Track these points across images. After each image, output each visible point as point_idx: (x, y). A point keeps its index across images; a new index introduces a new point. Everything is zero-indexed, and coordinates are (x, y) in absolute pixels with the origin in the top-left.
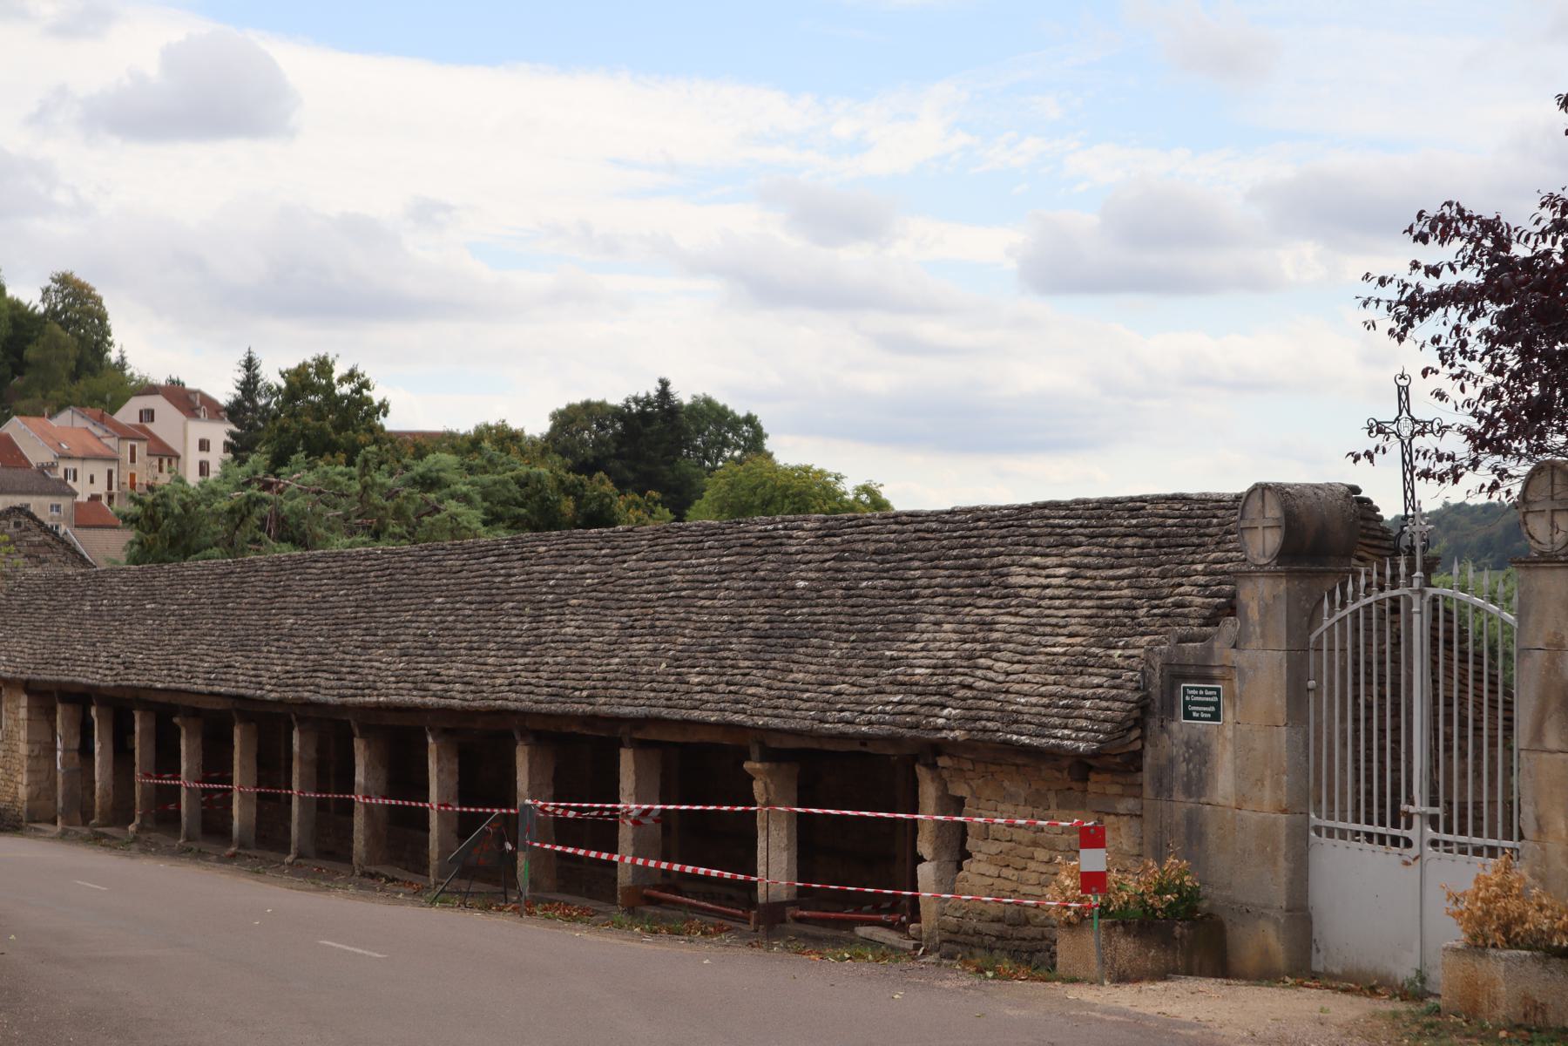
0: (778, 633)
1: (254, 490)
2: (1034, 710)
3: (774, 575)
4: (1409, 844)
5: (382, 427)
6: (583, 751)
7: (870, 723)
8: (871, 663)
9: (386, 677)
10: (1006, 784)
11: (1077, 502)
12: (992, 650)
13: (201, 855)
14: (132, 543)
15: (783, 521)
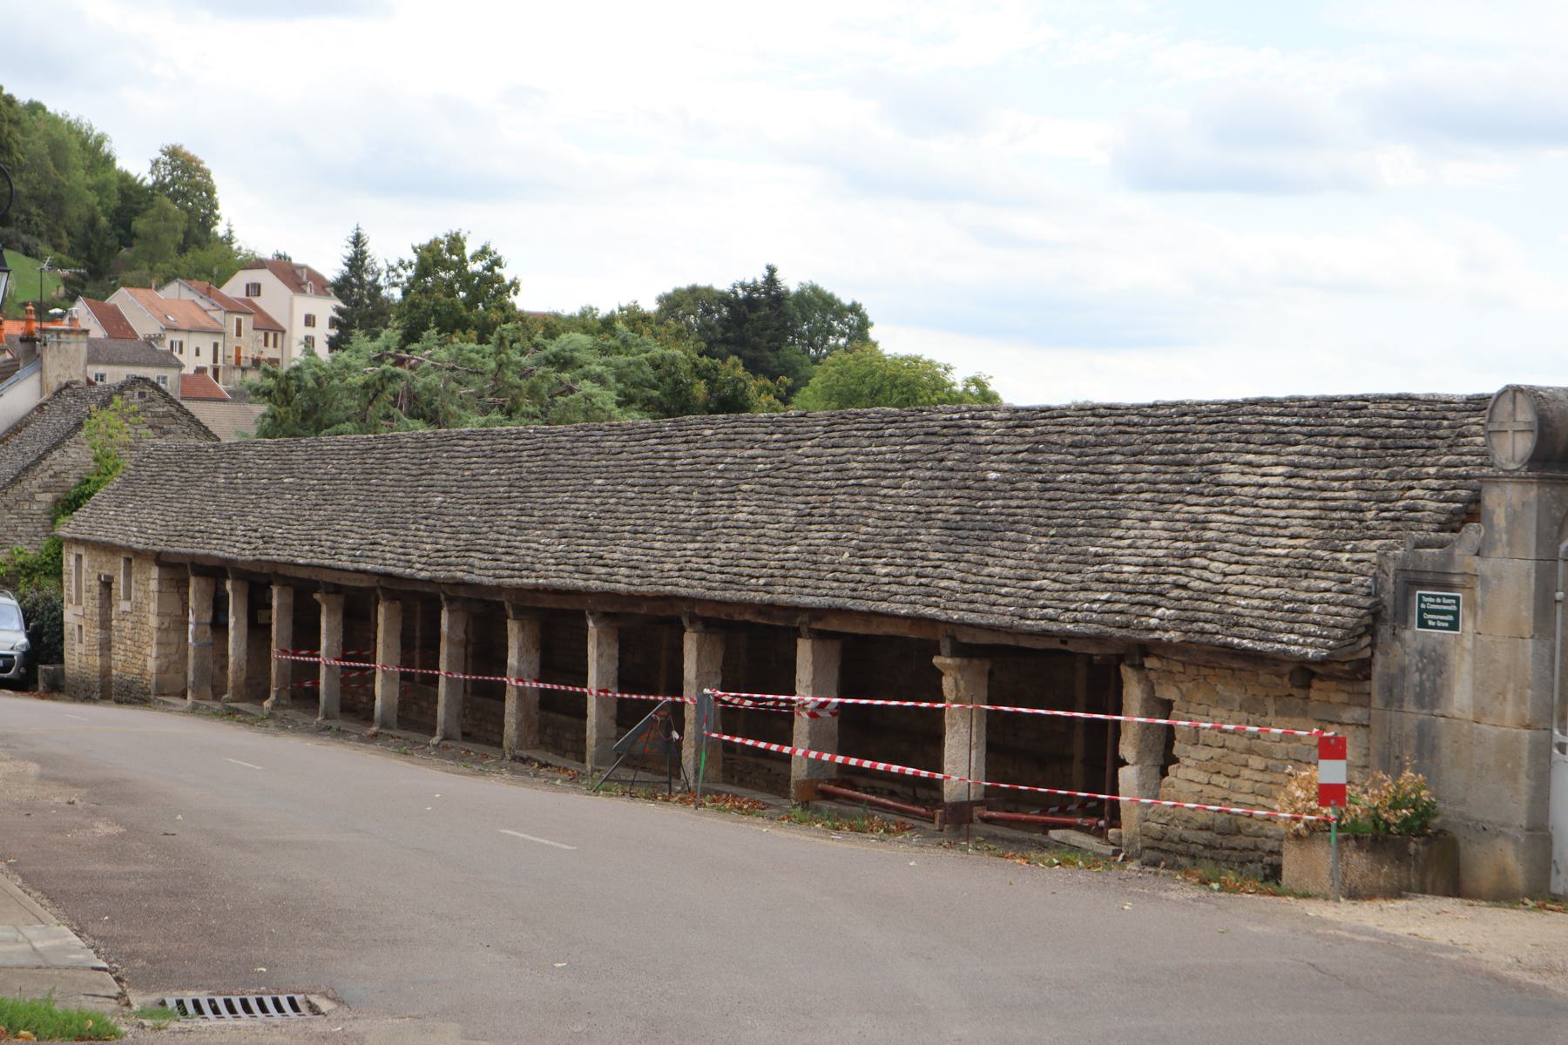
0: (970, 525)
1: (387, 366)
2: (1256, 613)
3: (962, 466)
5: (513, 306)
6: (756, 642)
7: (1075, 621)
8: (1073, 558)
9: (545, 559)
10: (1220, 688)
11: (1292, 399)
12: (1206, 549)
13: (340, 734)
14: (264, 416)
15: (969, 410)
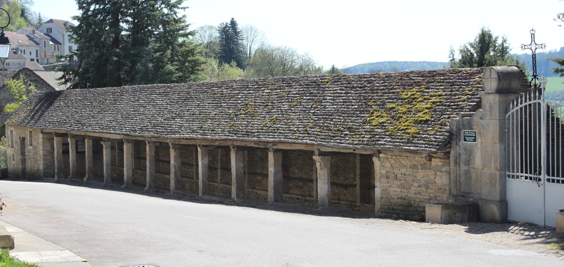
4: (540, 180)
